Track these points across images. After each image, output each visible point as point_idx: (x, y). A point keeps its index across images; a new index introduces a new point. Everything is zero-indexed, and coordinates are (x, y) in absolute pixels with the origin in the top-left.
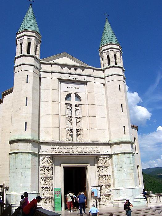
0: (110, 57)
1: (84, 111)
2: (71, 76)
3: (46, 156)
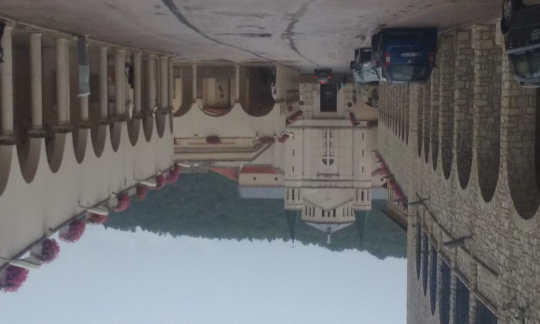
0: (233, 145)
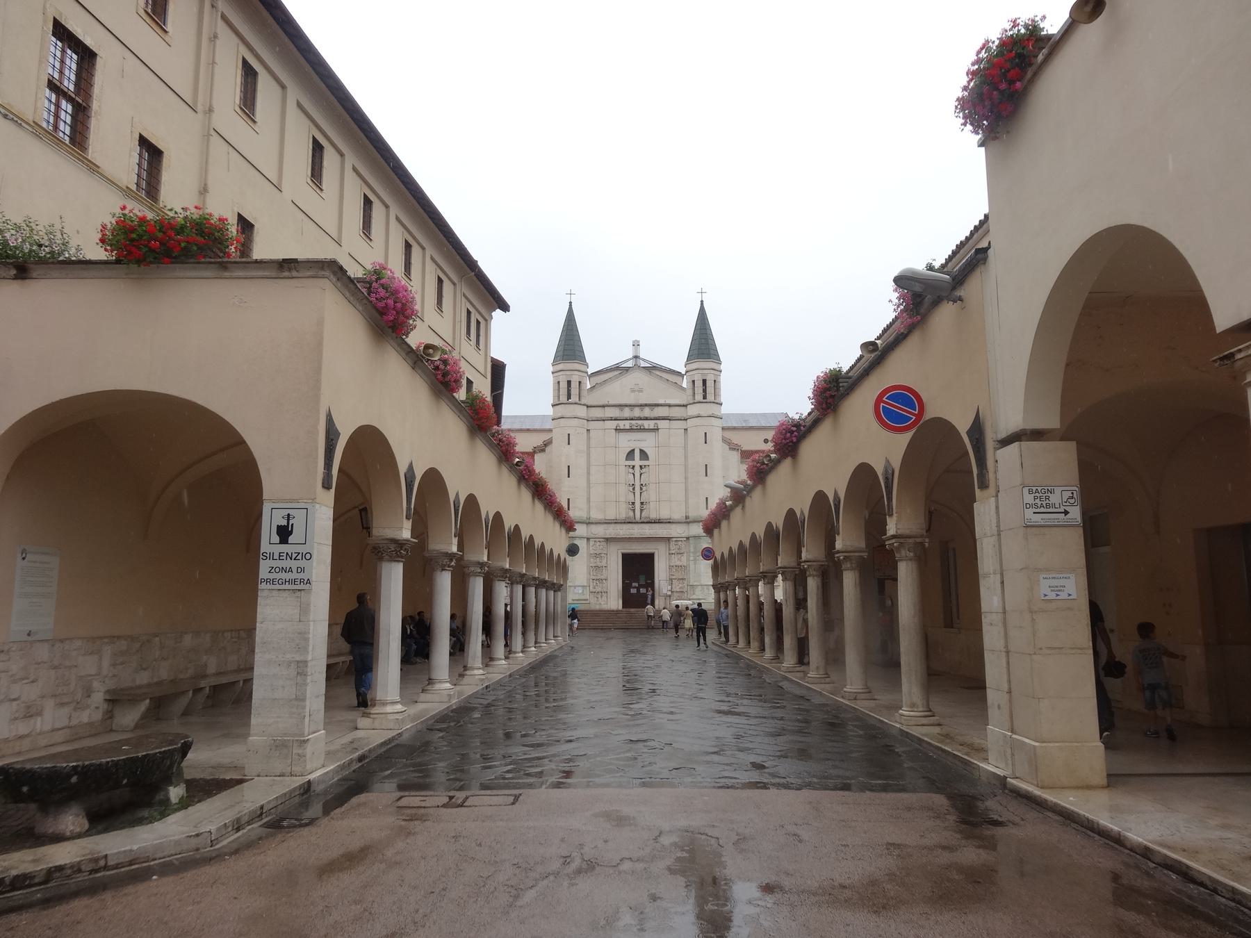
1: (650, 477)
2: (633, 422)
3: (597, 540)
